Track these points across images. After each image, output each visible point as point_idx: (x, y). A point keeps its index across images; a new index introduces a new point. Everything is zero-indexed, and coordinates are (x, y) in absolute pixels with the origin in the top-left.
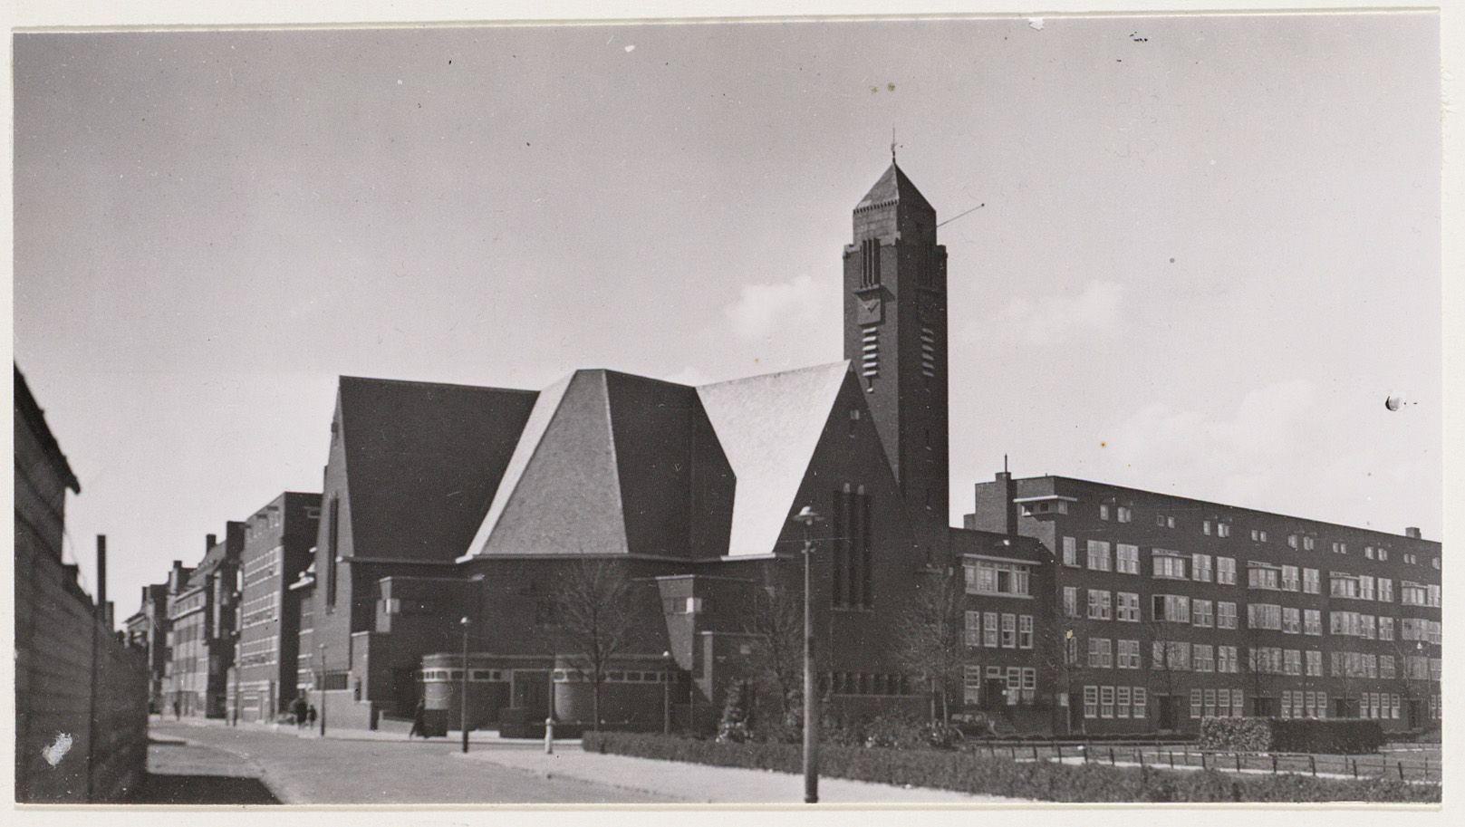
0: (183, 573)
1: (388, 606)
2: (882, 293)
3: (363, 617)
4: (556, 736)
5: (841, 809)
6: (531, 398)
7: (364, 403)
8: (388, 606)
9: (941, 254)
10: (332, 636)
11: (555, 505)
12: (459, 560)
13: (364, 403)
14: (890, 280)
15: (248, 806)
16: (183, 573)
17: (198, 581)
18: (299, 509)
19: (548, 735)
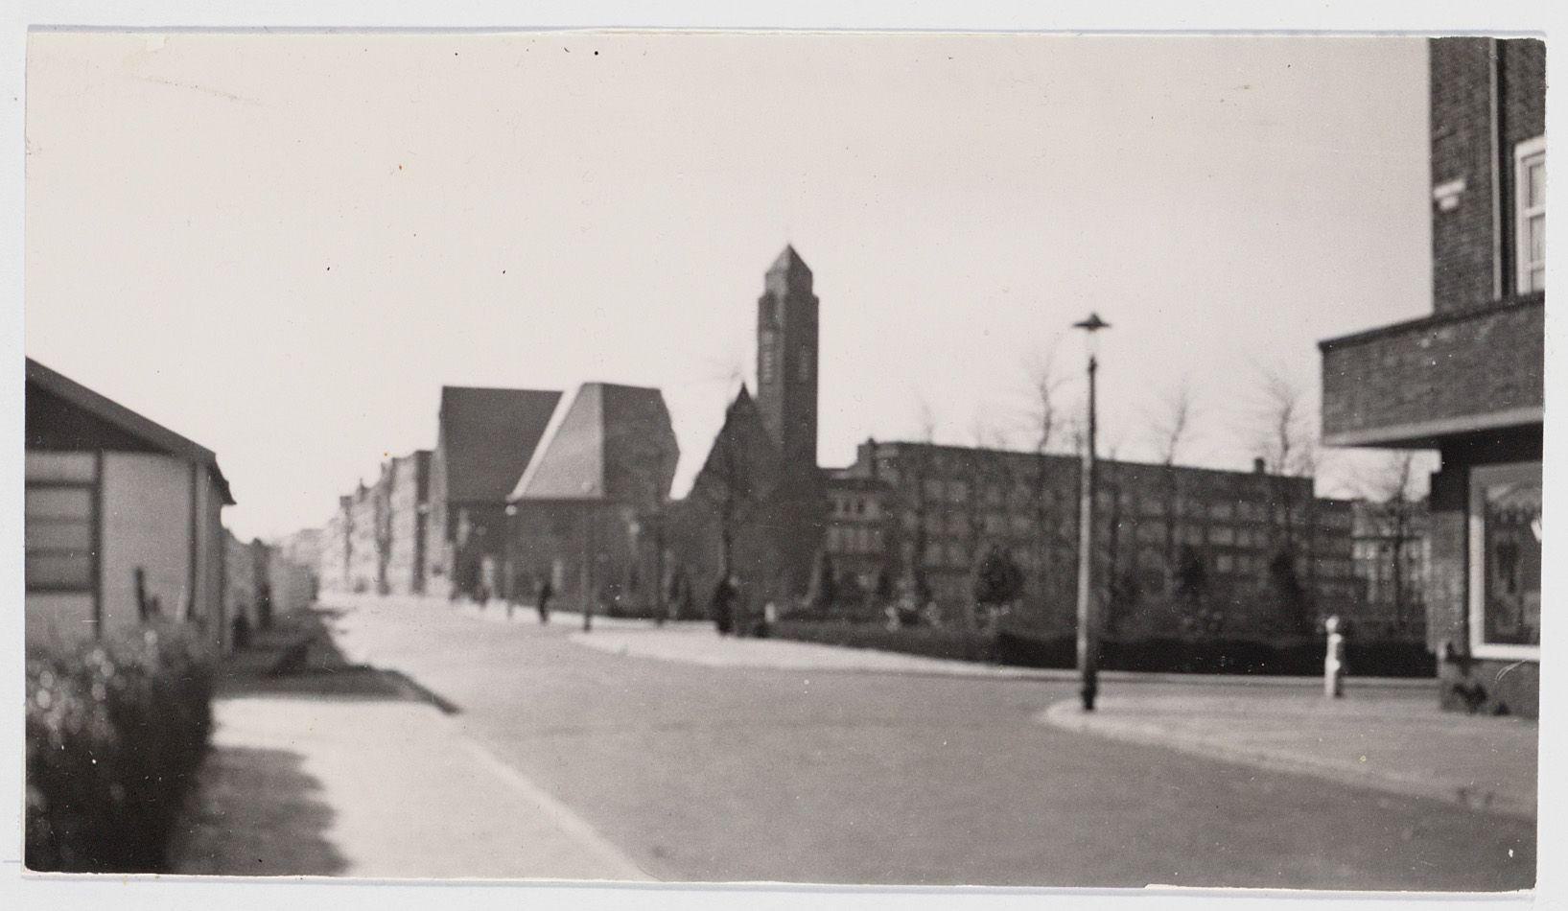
0: (363, 490)
1: (464, 528)
2: (775, 328)
3: (451, 535)
4: (1357, 662)
5: (757, 889)
6: (554, 397)
7: (455, 401)
8: (464, 528)
9: (815, 302)
10: (439, 550)
11: (562, 463)
12: (681, 487)
13: (455, 401)
14: (779, 317)
15: (1159, 676)
16: (363, 490)
17: (371, 495)
18: (423, 457)
19: (1332, 664)
